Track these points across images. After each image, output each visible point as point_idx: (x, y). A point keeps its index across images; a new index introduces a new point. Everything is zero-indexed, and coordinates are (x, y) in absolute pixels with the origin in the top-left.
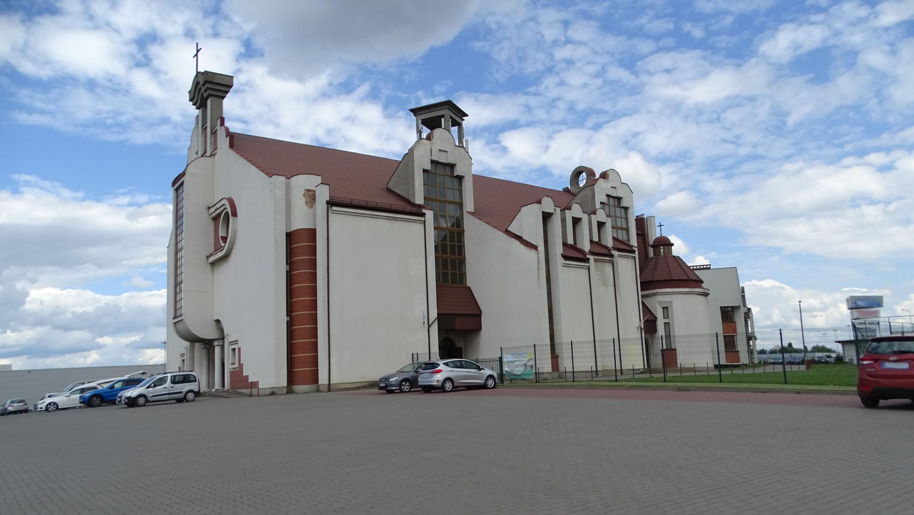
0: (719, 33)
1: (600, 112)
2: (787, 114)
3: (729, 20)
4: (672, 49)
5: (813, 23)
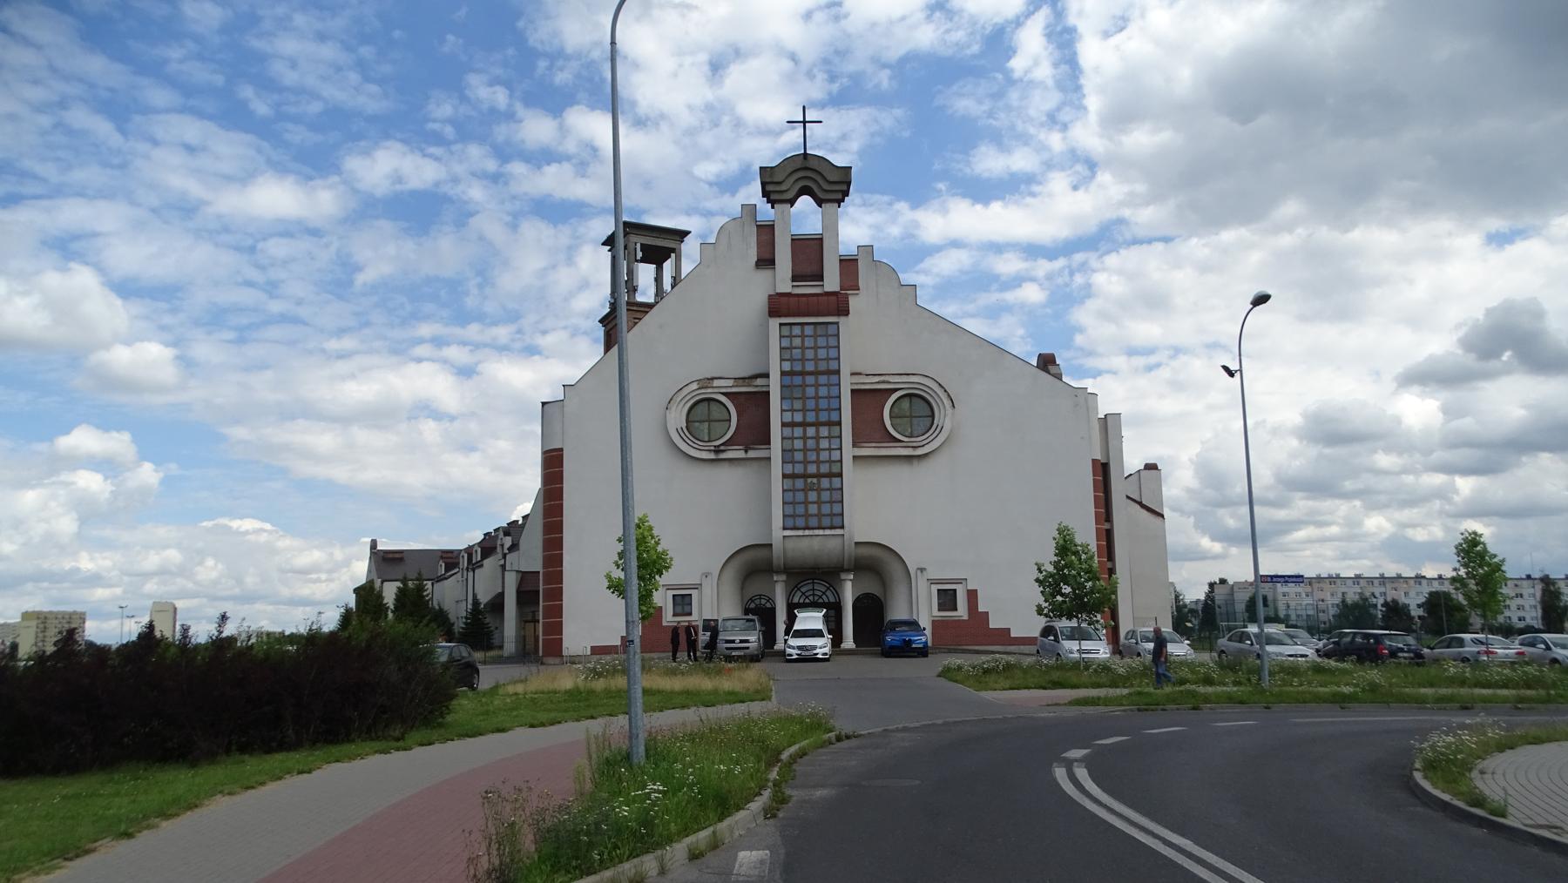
0: (297, 119)
1: (24, 175)
2: (358, 268)
3: (315, 107)
4: (210, 118)
5: (430, 156)
